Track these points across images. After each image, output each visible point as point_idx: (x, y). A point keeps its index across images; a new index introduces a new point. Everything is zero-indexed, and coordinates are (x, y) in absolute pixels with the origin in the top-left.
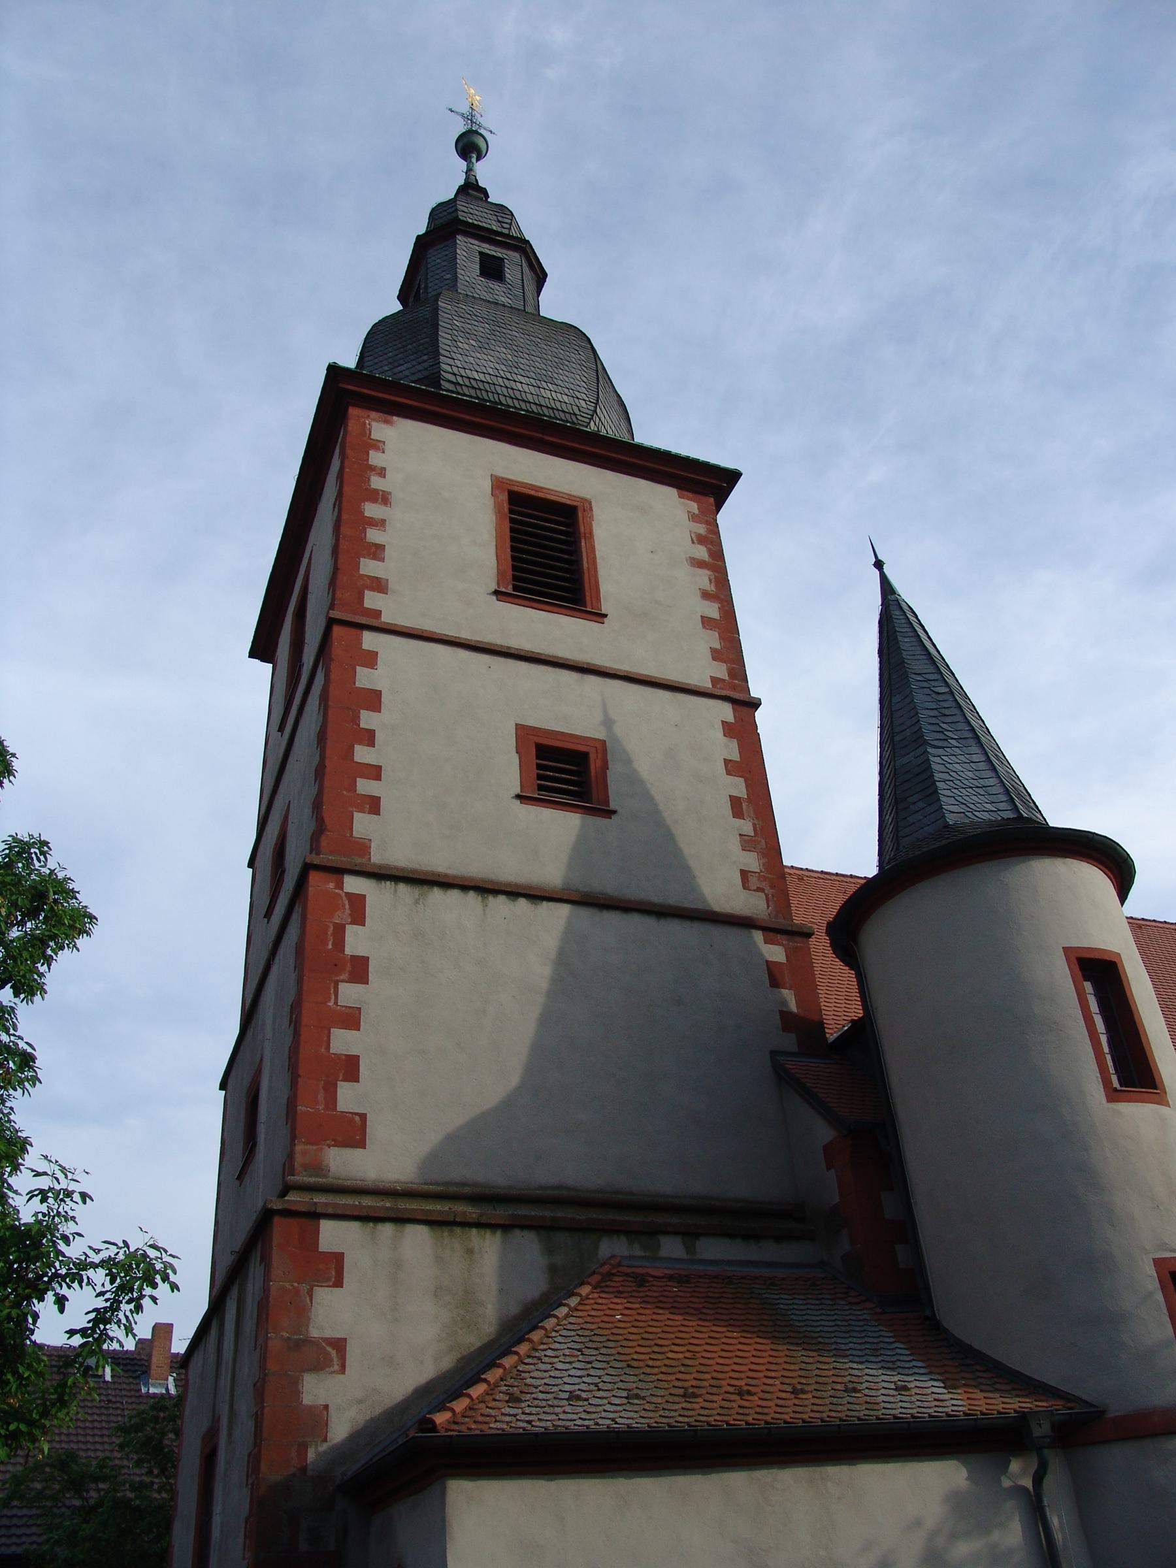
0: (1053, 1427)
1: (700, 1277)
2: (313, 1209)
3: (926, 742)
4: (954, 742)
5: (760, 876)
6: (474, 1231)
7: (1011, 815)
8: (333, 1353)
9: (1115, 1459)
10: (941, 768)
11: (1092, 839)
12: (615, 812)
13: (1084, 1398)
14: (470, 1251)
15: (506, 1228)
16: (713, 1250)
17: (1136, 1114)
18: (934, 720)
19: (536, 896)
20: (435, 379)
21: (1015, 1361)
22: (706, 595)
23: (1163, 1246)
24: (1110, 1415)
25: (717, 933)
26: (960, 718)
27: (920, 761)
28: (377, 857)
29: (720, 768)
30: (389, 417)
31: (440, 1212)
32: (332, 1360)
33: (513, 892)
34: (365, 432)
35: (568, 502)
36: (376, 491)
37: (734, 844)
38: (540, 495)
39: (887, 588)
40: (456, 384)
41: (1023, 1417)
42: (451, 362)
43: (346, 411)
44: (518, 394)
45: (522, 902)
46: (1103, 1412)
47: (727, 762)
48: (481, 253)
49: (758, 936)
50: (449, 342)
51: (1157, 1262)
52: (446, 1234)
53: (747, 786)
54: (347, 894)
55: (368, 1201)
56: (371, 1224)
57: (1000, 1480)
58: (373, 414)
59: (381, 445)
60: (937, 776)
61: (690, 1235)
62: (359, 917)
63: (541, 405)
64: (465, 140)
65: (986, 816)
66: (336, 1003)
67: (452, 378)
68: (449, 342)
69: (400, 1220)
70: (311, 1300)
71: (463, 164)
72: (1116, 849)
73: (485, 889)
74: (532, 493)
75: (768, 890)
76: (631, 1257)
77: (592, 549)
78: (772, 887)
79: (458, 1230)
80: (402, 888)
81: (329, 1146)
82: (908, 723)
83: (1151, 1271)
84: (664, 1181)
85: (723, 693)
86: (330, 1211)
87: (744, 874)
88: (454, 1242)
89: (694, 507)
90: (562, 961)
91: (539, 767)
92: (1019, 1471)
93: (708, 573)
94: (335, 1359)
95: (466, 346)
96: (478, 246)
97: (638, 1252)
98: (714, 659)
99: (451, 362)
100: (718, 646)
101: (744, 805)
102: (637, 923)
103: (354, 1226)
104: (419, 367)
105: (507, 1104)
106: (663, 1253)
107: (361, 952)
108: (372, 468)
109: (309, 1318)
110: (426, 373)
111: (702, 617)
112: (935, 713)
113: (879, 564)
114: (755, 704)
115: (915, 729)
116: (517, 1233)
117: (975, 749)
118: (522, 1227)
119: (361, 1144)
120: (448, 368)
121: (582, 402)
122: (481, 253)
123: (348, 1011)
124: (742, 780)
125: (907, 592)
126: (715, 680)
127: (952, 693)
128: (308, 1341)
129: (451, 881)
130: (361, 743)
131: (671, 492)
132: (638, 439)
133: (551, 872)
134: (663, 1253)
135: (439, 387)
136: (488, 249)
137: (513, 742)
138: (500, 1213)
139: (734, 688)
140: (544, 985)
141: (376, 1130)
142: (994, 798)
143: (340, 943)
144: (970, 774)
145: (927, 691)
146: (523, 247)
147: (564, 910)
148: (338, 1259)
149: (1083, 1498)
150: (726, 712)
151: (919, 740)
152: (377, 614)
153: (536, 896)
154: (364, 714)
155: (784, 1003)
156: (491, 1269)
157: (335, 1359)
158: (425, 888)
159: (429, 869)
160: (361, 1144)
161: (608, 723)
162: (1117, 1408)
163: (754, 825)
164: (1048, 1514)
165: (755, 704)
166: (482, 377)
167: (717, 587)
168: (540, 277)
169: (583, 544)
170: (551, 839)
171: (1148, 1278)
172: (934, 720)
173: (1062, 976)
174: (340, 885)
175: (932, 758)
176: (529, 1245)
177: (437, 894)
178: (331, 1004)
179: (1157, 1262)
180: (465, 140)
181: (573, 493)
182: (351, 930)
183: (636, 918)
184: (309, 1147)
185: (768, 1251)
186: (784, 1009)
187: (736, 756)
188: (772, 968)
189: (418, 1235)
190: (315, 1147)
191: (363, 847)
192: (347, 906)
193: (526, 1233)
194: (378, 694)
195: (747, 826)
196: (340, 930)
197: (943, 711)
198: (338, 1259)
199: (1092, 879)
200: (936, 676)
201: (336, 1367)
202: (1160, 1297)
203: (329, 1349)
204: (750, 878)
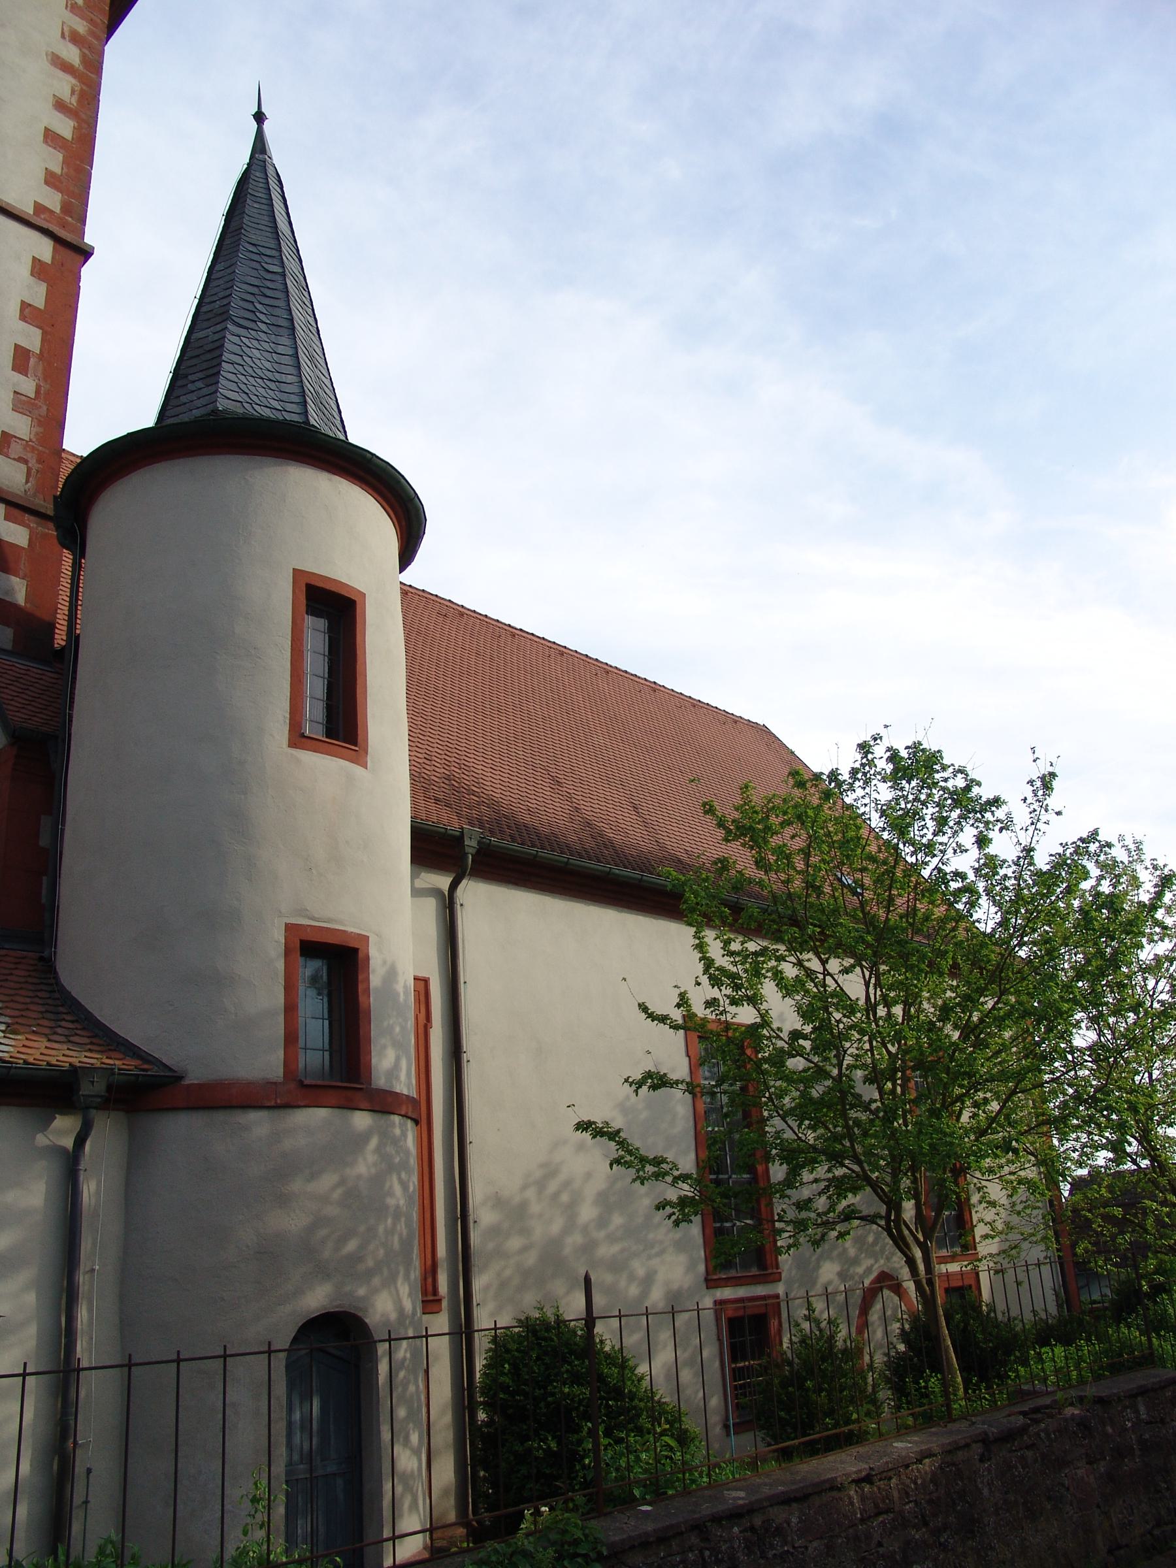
0: (109, 1088)
3: (229, 318)
4: (263, 327)
5: (27, 444)
7: (296, 418)
9: (178, 1130)
10: (236, 349)
11: (370, 461)
17: (324, 768)
18: (249, 297)
21: (105, 1014)
22: (60, 106)
23: (303, 912)
24: (187, 1082)
26: (281, 303)
27: (217, 337)
29: (14, 309)
39: (260, 146)
41: (74, 1070)
46: (181, 1078)
47: (24, 305)
51: (289, 927)
53: (43, 341)
57: (34, 1138)
60: (226, 356)
65: (266, 413)
72: (399, 482)
75: (33, 463)
78: (39, 461)
82: (221, 295)
83: (279, 936)
85: (45, 225)
92: (62, 1129)
93: (74, 81)
98: (47, 183)
100: (57, 170)
101: (32, 361)
111: (47, 130)
112: (255, 290)
113: (259, 117)
114: (86, 253)
115: (225, 302)
117: (285, 340)
124: (39, 332)
125: (280, 157)
126: (39, 208)
127: (284, 275)
142: (284, 397)
145: (257, 266)
149: (135, 1162)
150: (44, 249)
151: (224, 315)
155: (10, 591)
162: (196, 1075)
164: (81, 1178)
165: (86, 253)
167: (79, 101)
171: (273, 943)
172: (249, 297)
173: (281, 601)
175: (229, 336)
179: (289, 927)
187: (39, 302)
195: (28, 386)
199: (381, 529)
200: (273, 253)
202: (280, 965)
204: (13, 445)
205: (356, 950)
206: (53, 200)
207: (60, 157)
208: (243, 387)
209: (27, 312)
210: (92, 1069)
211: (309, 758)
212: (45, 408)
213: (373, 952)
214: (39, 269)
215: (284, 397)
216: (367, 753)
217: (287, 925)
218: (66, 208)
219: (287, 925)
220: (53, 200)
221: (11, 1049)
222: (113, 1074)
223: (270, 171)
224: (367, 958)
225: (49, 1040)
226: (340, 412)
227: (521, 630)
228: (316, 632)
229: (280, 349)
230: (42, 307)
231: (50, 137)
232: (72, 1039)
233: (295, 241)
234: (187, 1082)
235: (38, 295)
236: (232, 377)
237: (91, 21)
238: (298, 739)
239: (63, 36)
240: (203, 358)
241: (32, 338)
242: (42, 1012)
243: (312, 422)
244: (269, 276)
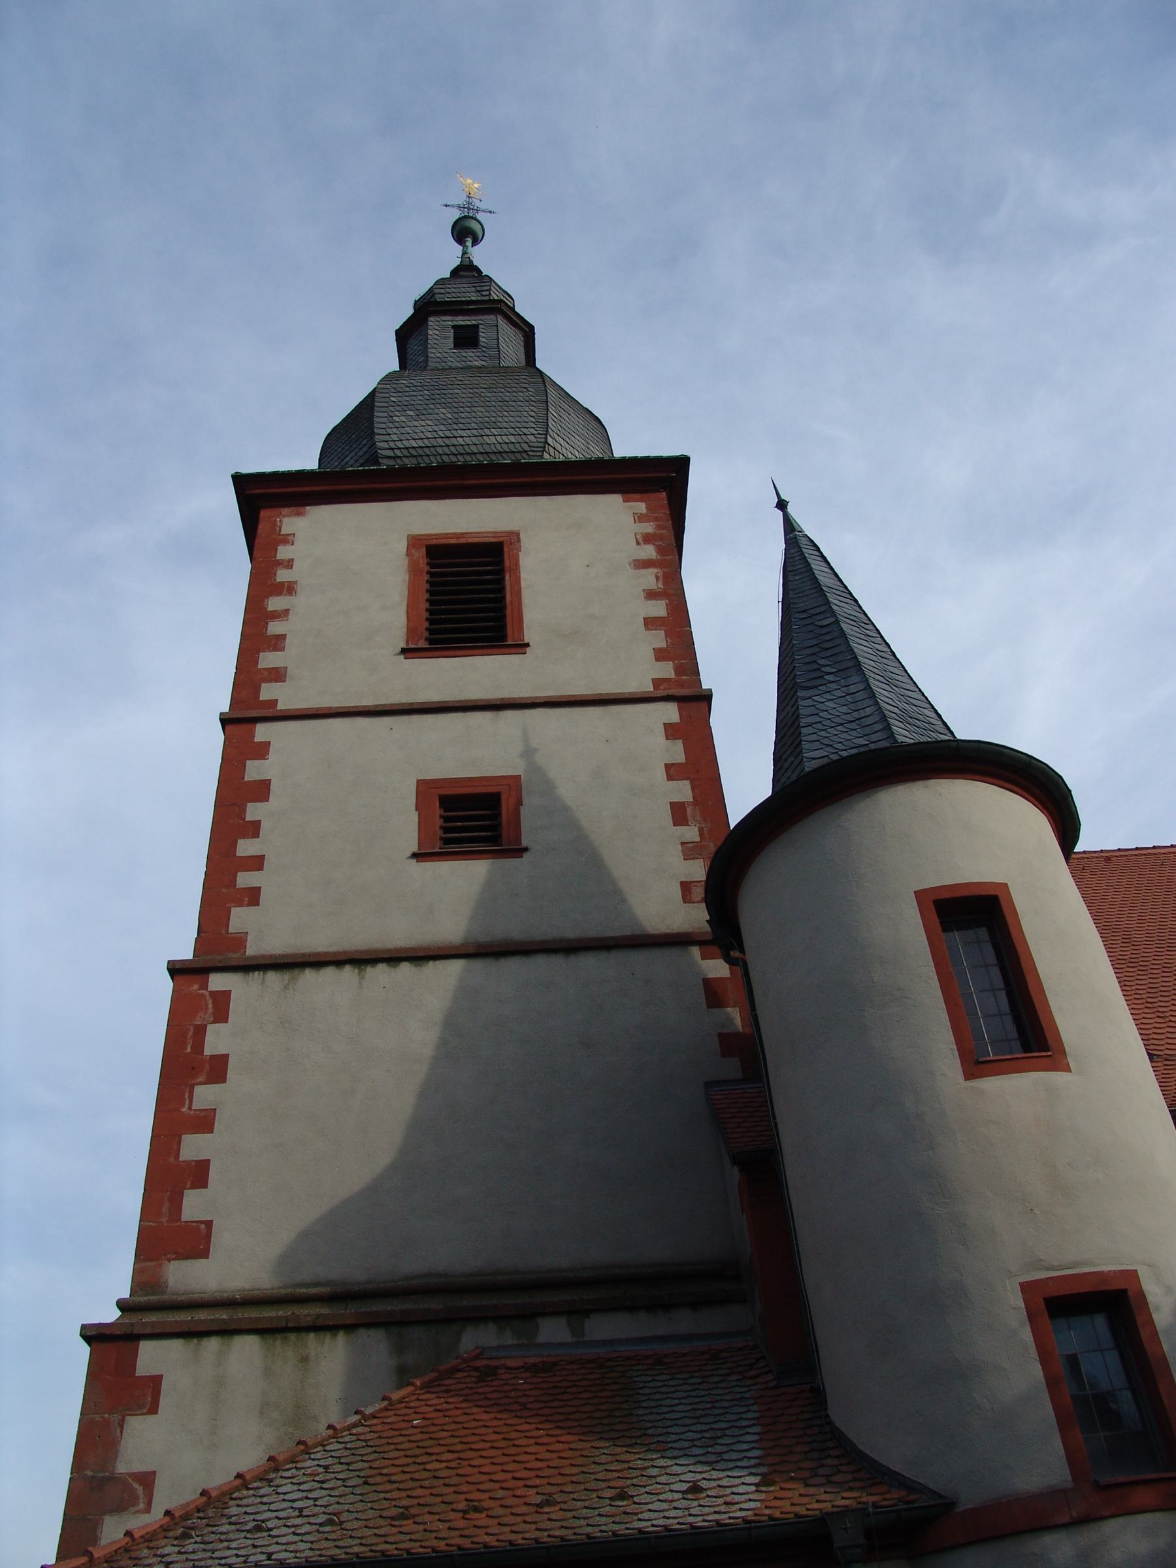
1: (572, 1363)
2: (128, 1331)
4: (831, 678)
6: (312, 1335)
8: (140, 1490)
12: (526, 849)
13: (932, 1486)
14: (305, 1359)
15: (349, 1328)
16: (605, 1328)
17: (1016, 1091)
18: (810, 659)
19: (419, 956)
20: (374, 459)
24: (960, 1509)
25: (638, 959)
28: (252, 950)
29: (661, 773)
30: (301, 509)
31: (270, 1319)
32: (137, 1497)
33: (393, 958)
34: (275, 528)
35: (493, 540)
36: (282, 583)
37: (674, 853)
38: (462, 541)
39: (790, 526)
40: (395, 457)
41: (823, 1520)
42: (387, 438)
43: (258, 514)
44: (461, 449)
45: (405, 967)
46: (953, 1504)
48: (453, 327)
49: (695, 951)
50: (385, 420)
51: (1025, 1287)
52: (278, 1343)
54: (212, 993)
55: (202, 1315)
56: (195, 1341)
58: (285, 511)
59: (291, 538)
61: (576, 1313)
62: (222, 1016)
63: (487, 453)
64: (458, 228)
66: (190, 1108)
67: (390, 453)
68: (385, 420)
69: (226, 1332)
70: (121, 1432)
71: (459, 249)
72: (1002, 754)
73: (361, 960)
74: (453, 541)
76: (499, 1348)
77: (518, 580)
79: (292, 1337)
80: (272, 976)
81: (169, 1260)
83: (1017, 1301)
84: (560, 1253)
85: (664, 693)
86: (148, 1330)
87: (686, 887)
88: (286, 1351)
89: (641, 507)
90: (450, 1023)
91: (446, 819)
94: (141, 1497)
95: (403, 419)
96: (449, 321)
97: (509, 1339)
99: (387, 438)
100: (663, 645)
101: (689, 810)
102: (541, 963)
103: (177, 1344)
104: (361, 453)
105: (373, 1190)
106: (542, 1338)
107: (221, 1051)
108: (279, 563)
109: (117, 1451)
110: (366, 456)
112: (816, 649)
113: (782, 505)
116: (362, 1332)
118: (368, 1326)
119: (205, 1254)
120: (385, 445)
121: (532, 438)
122: (453, 327)
123: (202, 1114)
125: (809, 526)
126: (657, 683)
128: (114, 1479)
129: (323, 959)
130: (244, 836)
131: (616, 499)
132: (619, 452)
133: (451, 928)
134: (542, 1338)
135: (379, 464)
136: (461, 320)
137: (412, 800)
138: (348, 1312)
139: (681, 684)
140: (428, 1052)
141: (221, 1239)
142: (868, 730)
143: (199, 1045)
144: (844, 709)
146: (503, 308)
147: (455, 967)
148: (155, 1382)
150: (670, 712)
152: (274, 702)
153: (419, 956)
154: (250, 807)
155: (730, 1021)
156: (333, 1375)
157: (141, 1497)
158: (296, 971)
159: (307, 951)
160: (205, 1254)
161: (528, 753)
162: (969, 1499)
163: (701, 830)
166: (420, 443)
167: (665, 583)
168: (528, 332)
169: (507, 577)
170: (456, 893)
173: (909, 932)
174: (205, 985)
176: (376, 1343)
177: (309, 975)
178: (184, 1110)
179: (1025, 1287)
180: (458, 228)
181: (499, 530)
182: (211, 1028)
183: (541, 960)
184: (148, 1264)
185: (683, 1322)
186: (725, 1031)
188: (708, 984)
189: (247, 1347)
190: (154, 1263)
191: (240, 941)
192: (210, 1006)
193: (372, 1332)
194: (670, 778)
196: (201, 1031)
197: (822, 646)
198: (155, 1382)
201: (142, 1506)
202: (1027, 1335)
203: (136, 1485)
205: (1124, 1292)
206: (666, 670)
207: (662, 633)
208: (826, 741)
209: (673, 772)
210: (846, 1511)
211: (992, 1084)
212: (712, 845)
213: (1151, 1288)
214: (671, 731)
215: (868, 730)
216: (1064, 1053)
217: (1022, 1285)
218: (679, 670)
219: (1022, 1285)
220: (666, 670)
221: (758, 1504)
222: (868, 1515)
223: (803, 541)
224: (1141, 1295)
225: (807, 1485)
226: (939, 716)
227: (1137, 849)
228: (972, 948)
229: (853, 689)
230: (246, 779)
231: (650, 623)
232: (833, 1479)
233: (846, 587)
234: (960, 1509)
235: (677, 752)
236: (814, 737)
237: (657, 519)
238: (976, 1065)
239: (638, 543)
240: (788, 734)
241: (683, 791)
242: (805, 1453)
243: (900, 739)
244: (824, 631)
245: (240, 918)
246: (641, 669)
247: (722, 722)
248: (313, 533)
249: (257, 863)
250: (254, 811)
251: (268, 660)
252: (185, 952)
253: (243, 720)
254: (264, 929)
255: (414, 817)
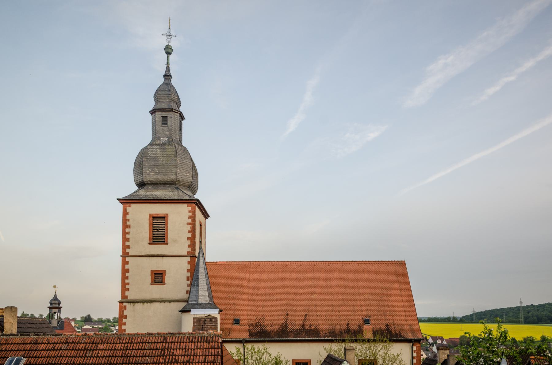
89: (190, 208)
131: (186, 205)
136: (164, 114)
150: (189, 259)
191: (127, 297)
218: (192, 250)
245: (127, 293)
246: (185, 250)
247: (199, 247)
248: (133, 209)
249: (128, 284)
250: (127, 274)
251: (127, 281)
252: (120, 299)
253: (125, 255)
254: (131, 295)
255: (145, 332)
